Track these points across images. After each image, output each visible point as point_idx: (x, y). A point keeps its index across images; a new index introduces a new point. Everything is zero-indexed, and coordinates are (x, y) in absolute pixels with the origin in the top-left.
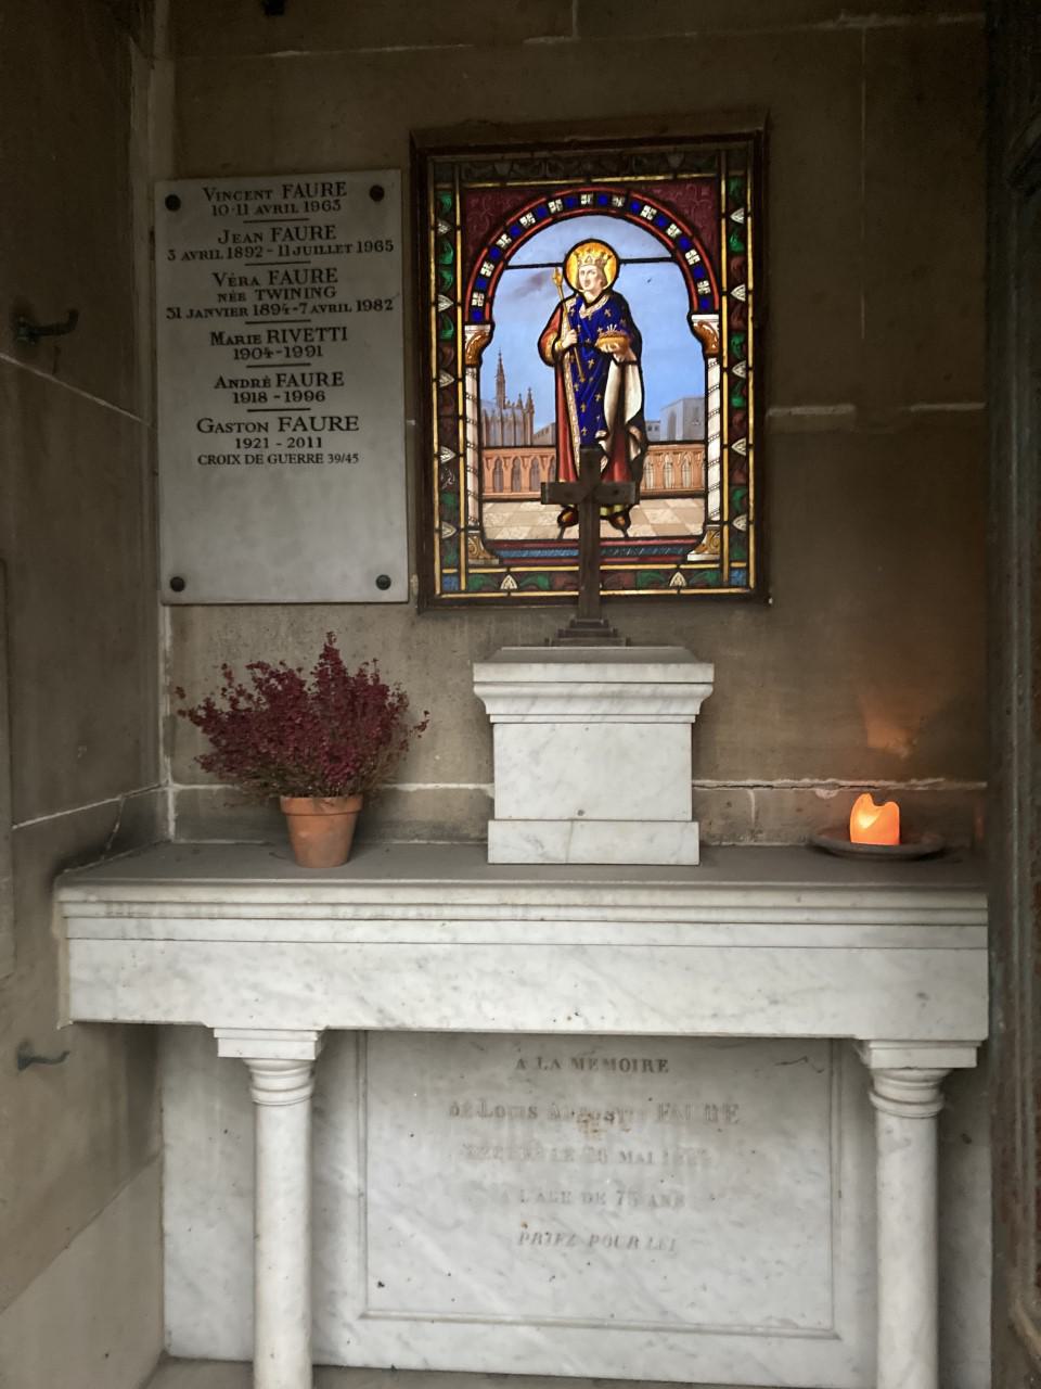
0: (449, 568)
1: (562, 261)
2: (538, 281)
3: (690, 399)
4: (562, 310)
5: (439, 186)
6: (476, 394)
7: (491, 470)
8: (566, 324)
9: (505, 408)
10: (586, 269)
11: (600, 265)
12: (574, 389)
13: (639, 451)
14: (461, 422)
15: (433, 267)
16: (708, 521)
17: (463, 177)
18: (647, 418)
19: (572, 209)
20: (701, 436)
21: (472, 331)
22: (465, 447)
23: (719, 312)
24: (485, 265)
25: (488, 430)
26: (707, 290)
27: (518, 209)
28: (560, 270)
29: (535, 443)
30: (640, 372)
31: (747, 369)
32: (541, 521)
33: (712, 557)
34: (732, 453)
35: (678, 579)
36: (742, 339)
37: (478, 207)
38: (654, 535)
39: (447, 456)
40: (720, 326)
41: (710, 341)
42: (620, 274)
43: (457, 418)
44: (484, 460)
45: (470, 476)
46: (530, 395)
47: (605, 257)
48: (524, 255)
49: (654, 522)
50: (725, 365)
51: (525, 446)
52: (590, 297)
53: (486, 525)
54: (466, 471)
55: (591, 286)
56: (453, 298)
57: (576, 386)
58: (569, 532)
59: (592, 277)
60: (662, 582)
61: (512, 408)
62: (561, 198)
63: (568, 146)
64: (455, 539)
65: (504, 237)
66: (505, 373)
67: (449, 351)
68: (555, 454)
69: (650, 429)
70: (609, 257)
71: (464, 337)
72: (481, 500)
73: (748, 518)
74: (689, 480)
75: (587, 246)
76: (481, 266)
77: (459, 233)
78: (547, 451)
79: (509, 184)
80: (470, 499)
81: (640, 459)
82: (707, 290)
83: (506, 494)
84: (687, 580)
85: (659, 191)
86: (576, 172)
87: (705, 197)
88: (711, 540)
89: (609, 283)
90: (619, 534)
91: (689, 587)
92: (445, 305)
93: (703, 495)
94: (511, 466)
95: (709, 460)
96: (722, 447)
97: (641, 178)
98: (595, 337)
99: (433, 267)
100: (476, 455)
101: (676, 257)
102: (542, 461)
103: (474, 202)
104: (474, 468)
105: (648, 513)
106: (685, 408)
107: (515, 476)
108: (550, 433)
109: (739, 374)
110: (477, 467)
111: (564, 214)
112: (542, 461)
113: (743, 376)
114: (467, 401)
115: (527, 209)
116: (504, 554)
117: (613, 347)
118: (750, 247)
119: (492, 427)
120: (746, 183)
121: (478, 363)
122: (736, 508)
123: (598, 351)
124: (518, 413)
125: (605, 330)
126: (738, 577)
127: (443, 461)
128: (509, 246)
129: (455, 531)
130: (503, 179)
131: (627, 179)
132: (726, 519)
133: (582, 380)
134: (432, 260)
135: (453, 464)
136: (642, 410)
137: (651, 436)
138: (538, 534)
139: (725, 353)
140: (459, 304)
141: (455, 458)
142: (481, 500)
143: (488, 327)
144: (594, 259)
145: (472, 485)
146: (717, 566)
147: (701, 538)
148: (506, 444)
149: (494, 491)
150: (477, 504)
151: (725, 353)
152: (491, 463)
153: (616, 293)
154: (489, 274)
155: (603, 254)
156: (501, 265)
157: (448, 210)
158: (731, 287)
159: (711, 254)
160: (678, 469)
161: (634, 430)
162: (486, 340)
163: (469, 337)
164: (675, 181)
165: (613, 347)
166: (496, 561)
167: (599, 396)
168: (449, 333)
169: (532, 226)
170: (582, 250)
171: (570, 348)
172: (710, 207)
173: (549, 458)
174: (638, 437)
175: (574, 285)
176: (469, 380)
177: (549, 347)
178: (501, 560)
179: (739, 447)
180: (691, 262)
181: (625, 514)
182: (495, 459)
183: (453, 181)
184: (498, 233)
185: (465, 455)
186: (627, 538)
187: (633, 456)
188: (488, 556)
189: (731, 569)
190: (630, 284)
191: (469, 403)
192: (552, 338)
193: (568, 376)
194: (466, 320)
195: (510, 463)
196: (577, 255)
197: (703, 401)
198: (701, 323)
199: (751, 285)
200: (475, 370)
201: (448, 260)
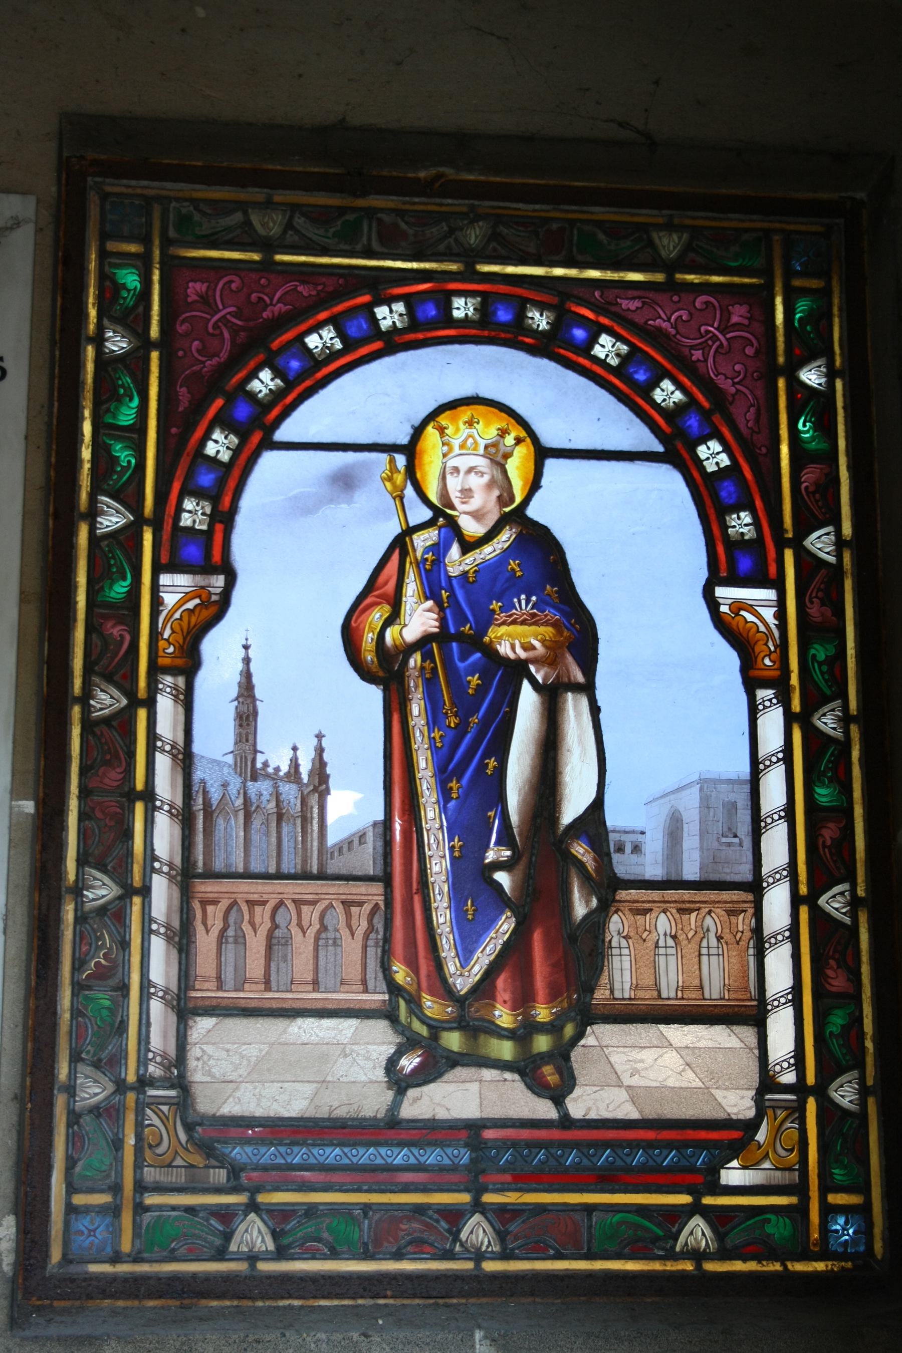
0: (91, 1191)
1: (404, 440)
2: (345, 482)
3: (716, 782)
4: (404, 554)
5: (111, 246)
6: (181, 741)
7: (215, 932)
8: (411, 588)
9: (254, 779)
10: (463, 463)
11: (497, 458)
12: (432, 740)
13: (594, 902)
14: (139, 808)
15: (87, 428)
16: (767, 1083)
17: (172, 233)
18: (613, 818)
19: (428, 329)
20: (744, 873)
21: (176, 587)
22: (149, 870)
23: (779, 586)
24: (217, 435)
25: (209, 831)
26: (749, 533)
27: (304, 315)
28: (401, 460)
29: (333, 867)
30: (595, 710)
31: (846, 720)
32: (341, 1069)
33: (779, 1177)
34: (819, 918)
35: (697, 1232)
36: (832, 651)
37: (206, 301)
38: (635, 1115)
39: (101, 890)
40: (781, 615)
41: (760, 647)
42: (544, 482)
43: (132, 796)
44: (196, 905)
45: (158, 945)
46: (320, 750)
47: (509, 440)
48: (307, 421)
49: (635, 1081)
50: (796, 706)
51: (305, 876)
52: (472, 528)
53: (197, 1074)
54: (147, 933)
55: (476, 503)
56: (133, 502)
57: (436, 734)
58: (416, 1100)
59: (477, 482)
60: (656, 1239)
61: (274, 777)
62: (407, 299)
63: (425, 189)
64: (108, 1112)
65: (266, 375)
66: (258, 693)
67: (116, 631)
68: (380, 900)
69: (620, 849)
70: (519, 441)
71: (157, 602)
72: (185, 1009)
73: (862, 1080)
74: (716, 979)
75: (466, 413)
76: (207, 437)
77: (155, 355)
78: (361, 889)
79: (279, 257)
80: (156, 1007)
81: (596, 922)
82: (749, 533)
83: (252, 994)
84: (720, 1236)
85: (634, 305)
86: (441, 247)
87: (737, 326)
88: (776, 1133)
89: (518, 499)
90: (545, 1110)
91: (724, 1254)
92: (112, 520)
93: (753, 1015)
94: (268, 924)
95: (767, 931)
96: (796, 901)
97: (594, 274)
98: (486, 621)
99: (87, 428)
100: (176, 894)
101: (676, 452)
102: (349, 916)
103: (195, 289)
104: (168, 927)
105: (618, 1059)
106: (705, 803)
107: (278, 950)
108: (369, 847)
109: (845, 1103)
110: (176, 924)
111: (412, 336)
112: (349, 916)
113: (839, 734)
114: (159, 756)
115: (323, 316)
116: (238, 1153)
117: (528, 647)
118: (842, 443)
119: (220, 823)
120: (830, 305)
121: (189, 663)
122: (832, 1051)
123: (490, 652)
124: (289, 791)
125: (507, 607)
126: (843, 1229)
127: (88, 906)
128: (276, 396)
129: (111, 1087)
130: (268, 246)
131: (559, 272)
132: (811, 1079)
133: (453, 721)
134: (87, 413)
135: (114, 912)
136: (598, 805)
137: (624, 866)
138: (334, 1104)
139: (794, 680)
140: (148, 522)
141: (120, 898)
142: (185, 1009)
143: (219, 581)
144: (482, 444)
145: (161, 965)
146: (794, 1200)
147: (752, 1126)
148: (256, 866)
149: (220, 988)
150: (173, 1018)
151: (794, 680)
152: (215, 913)
153: (535, 524)
154: (225, 456)
155: (503, 433)
156: (256, 438)
157: (130, 302)
158: (804, 527)
159: (754, 450)
160: (690, 949)
161: (580, 850)
162: (213, 610)
163: (170, 599)
164: (671, 287)
165: (528, 647)
166: (220, 1176)
167: (492, 763)
168: (120, 588)
169: (334, 355)
170: (454, 420)
171: (423, 643)
172: (749, 351)
173: (367, 908)
174: (590, 864)
175: (433, 497)
176: (165, 705)
177: (369, 639)
178: (235, 1171)
179: (833, 903)
180: (710, 467)
181: (561, 1056)
182: (224, 904)
183: (146, 241)
184: (252, 364)
185: (145, 891)
186: (566, 1121)
187: (580, 910)
188: (198, 1159)
189: (828, 1211)
190: (564, 503)
191: (163, 762)
192: (377, 616)
193: (417, 708)
194: (164, 559)
195: (263, 915)
196: (442, 430)
197: (747, 788)
198: (738, 606)
199: (847, 529)
200: (181, 681)
201: (126, 416)
